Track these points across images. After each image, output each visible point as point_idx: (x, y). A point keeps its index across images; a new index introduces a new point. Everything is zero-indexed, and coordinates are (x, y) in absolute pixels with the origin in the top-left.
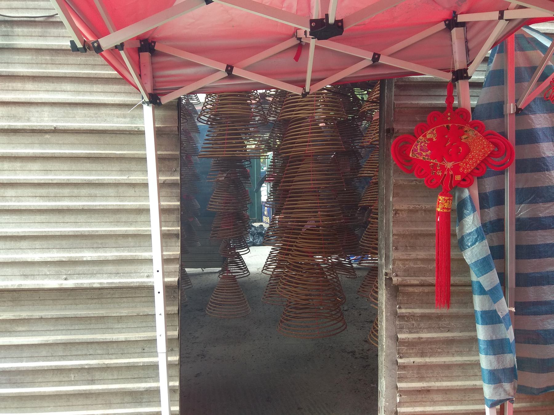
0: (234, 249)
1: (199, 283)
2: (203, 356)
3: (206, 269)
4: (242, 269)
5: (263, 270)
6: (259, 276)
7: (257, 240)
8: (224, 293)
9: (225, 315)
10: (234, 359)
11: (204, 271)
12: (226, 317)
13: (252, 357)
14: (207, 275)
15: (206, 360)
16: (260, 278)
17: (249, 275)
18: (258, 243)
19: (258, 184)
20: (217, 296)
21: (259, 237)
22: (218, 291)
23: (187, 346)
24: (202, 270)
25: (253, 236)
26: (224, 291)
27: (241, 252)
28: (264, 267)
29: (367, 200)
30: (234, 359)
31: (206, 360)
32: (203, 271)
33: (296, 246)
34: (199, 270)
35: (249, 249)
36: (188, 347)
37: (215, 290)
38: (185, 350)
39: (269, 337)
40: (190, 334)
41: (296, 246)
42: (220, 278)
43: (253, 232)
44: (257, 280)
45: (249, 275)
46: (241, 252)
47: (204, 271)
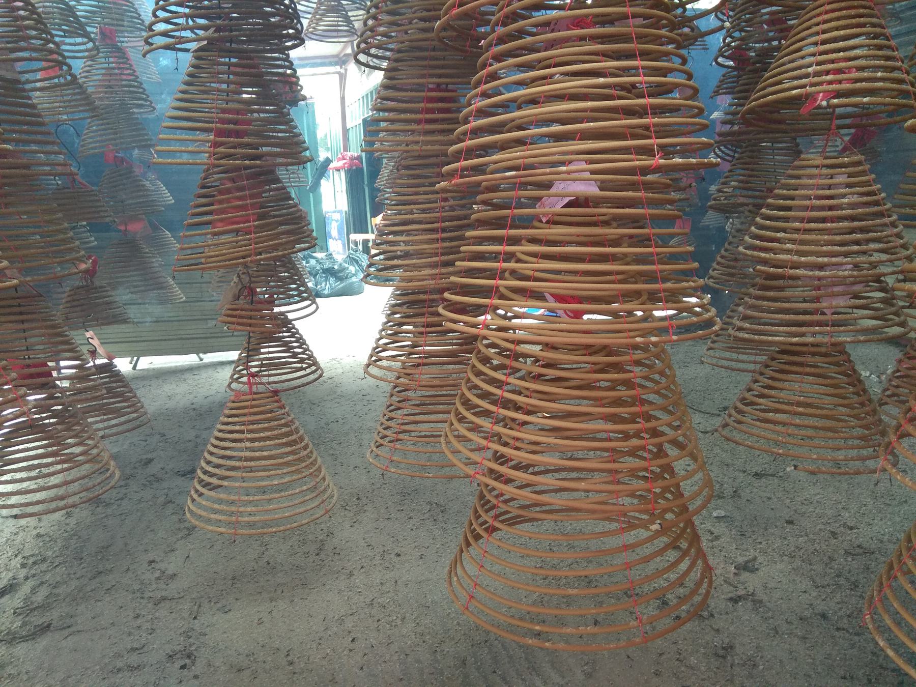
0: (271, 303)
1: (190, 393)
2: (189, 657)
3: (209, 355)
4: (295, 355)
5: (368, 365)
6: (338, 366)
7: (323, 285)
8: (241, 450)
9: (251, 525)
10: (291, 663)
11: (204, 361)
12: (286, 252)
13: (352, 646)
14: (210, 372)
15: (196, 677)
16: (341, 371)
17: (321, 376)
18: (326, 292)
19: (314, 175)
20: (228, 453)
21: (326, 277)
22: (222, 444)
23: (138, 616)
24: (199, 357)
25: (315, 276)
26: (242, 445)
27: (292, 311)
28: (371, 356)
29: (807, 76)
30: (291, 663)
31: (196, 677)
32: (201, 360)
33: (514, 273)
34: (191, 359)
35: (314, 302)
36: (139, 621)
37: (219, 426)
38: (130, 634)
39: (392, 556)
40: (151, 562)
41: (514, 273)
42: (232, 390)
43: (314, 268)
44: (334, 375)
45: (321, 376)
46: (292, 311)
47: (204, 361)
